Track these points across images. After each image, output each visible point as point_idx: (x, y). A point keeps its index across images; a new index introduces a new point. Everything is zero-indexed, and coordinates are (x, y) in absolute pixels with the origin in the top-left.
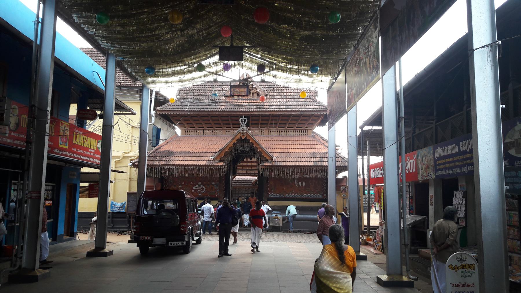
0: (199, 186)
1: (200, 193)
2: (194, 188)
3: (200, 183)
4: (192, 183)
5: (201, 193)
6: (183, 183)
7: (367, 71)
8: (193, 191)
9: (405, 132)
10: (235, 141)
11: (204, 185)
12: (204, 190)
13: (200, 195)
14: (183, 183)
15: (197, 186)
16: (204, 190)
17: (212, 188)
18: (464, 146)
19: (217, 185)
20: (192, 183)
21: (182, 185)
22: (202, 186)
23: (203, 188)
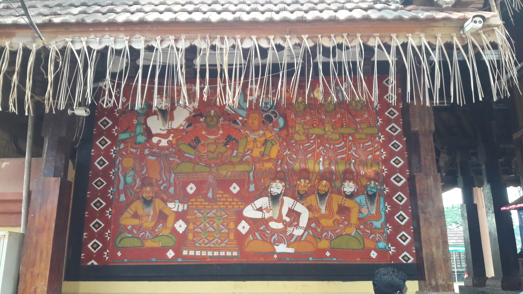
0: (275, 199)
1: (283, 236)
2: (249, 212)
3: (277, 187)
4: (235, 189)
5: (289, 240)
6: (191, 189)
7: (155, 61)
8: (244, 227)
9: (209, 54)
10: (171, 49)
11: (300, 197)
12: (304, 221)
13: (281, 248)
14: (191, 189)
15: (263, 202)
16: (304, 221)
17: (343, 210)
18: (96, 86)
19: (371, 198)
20: (235, 189)
21: (185, 198)
22: (288, 202)
23: (294, 215)
